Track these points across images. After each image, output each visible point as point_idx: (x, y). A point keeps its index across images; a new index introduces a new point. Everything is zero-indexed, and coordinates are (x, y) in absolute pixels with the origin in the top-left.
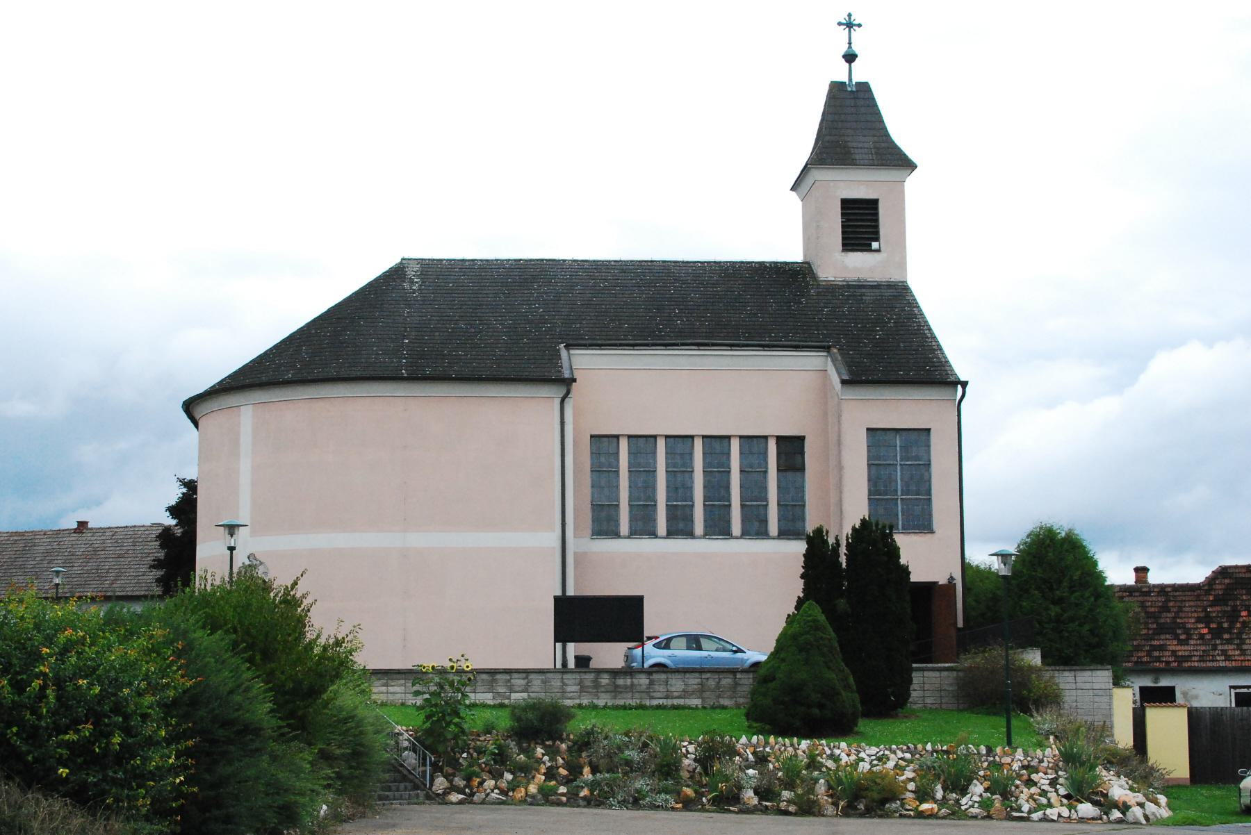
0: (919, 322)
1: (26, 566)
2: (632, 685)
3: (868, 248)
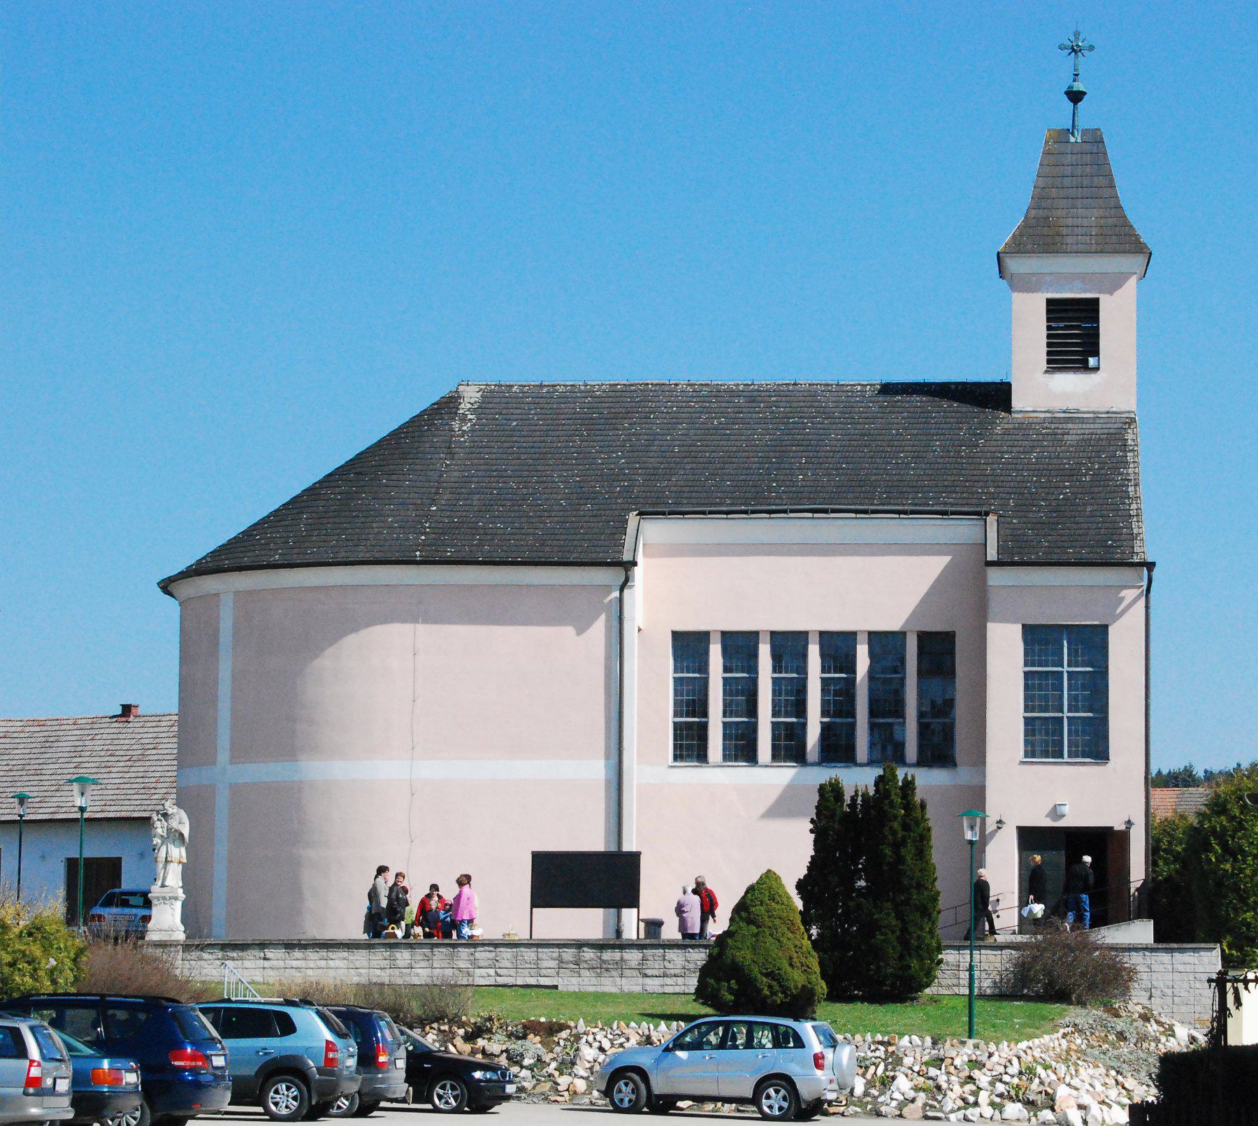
0: (1128, 474)
1: (43, 772)
2: (622, 959)
3: (1085, 368)
